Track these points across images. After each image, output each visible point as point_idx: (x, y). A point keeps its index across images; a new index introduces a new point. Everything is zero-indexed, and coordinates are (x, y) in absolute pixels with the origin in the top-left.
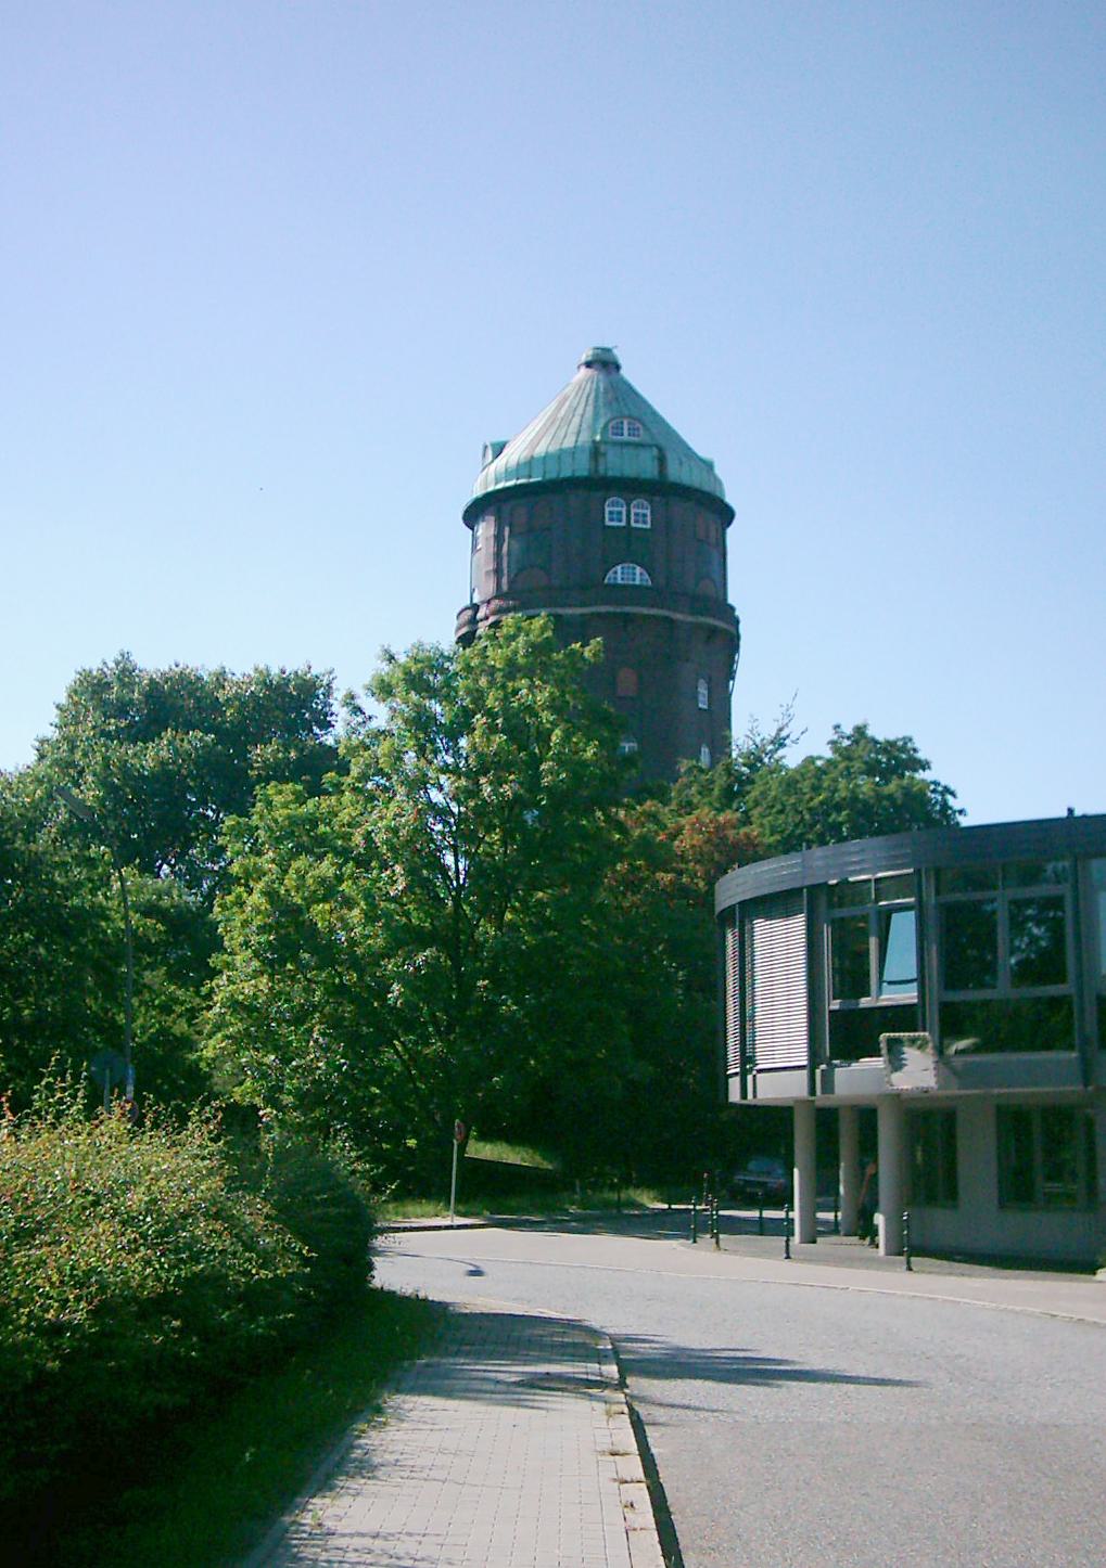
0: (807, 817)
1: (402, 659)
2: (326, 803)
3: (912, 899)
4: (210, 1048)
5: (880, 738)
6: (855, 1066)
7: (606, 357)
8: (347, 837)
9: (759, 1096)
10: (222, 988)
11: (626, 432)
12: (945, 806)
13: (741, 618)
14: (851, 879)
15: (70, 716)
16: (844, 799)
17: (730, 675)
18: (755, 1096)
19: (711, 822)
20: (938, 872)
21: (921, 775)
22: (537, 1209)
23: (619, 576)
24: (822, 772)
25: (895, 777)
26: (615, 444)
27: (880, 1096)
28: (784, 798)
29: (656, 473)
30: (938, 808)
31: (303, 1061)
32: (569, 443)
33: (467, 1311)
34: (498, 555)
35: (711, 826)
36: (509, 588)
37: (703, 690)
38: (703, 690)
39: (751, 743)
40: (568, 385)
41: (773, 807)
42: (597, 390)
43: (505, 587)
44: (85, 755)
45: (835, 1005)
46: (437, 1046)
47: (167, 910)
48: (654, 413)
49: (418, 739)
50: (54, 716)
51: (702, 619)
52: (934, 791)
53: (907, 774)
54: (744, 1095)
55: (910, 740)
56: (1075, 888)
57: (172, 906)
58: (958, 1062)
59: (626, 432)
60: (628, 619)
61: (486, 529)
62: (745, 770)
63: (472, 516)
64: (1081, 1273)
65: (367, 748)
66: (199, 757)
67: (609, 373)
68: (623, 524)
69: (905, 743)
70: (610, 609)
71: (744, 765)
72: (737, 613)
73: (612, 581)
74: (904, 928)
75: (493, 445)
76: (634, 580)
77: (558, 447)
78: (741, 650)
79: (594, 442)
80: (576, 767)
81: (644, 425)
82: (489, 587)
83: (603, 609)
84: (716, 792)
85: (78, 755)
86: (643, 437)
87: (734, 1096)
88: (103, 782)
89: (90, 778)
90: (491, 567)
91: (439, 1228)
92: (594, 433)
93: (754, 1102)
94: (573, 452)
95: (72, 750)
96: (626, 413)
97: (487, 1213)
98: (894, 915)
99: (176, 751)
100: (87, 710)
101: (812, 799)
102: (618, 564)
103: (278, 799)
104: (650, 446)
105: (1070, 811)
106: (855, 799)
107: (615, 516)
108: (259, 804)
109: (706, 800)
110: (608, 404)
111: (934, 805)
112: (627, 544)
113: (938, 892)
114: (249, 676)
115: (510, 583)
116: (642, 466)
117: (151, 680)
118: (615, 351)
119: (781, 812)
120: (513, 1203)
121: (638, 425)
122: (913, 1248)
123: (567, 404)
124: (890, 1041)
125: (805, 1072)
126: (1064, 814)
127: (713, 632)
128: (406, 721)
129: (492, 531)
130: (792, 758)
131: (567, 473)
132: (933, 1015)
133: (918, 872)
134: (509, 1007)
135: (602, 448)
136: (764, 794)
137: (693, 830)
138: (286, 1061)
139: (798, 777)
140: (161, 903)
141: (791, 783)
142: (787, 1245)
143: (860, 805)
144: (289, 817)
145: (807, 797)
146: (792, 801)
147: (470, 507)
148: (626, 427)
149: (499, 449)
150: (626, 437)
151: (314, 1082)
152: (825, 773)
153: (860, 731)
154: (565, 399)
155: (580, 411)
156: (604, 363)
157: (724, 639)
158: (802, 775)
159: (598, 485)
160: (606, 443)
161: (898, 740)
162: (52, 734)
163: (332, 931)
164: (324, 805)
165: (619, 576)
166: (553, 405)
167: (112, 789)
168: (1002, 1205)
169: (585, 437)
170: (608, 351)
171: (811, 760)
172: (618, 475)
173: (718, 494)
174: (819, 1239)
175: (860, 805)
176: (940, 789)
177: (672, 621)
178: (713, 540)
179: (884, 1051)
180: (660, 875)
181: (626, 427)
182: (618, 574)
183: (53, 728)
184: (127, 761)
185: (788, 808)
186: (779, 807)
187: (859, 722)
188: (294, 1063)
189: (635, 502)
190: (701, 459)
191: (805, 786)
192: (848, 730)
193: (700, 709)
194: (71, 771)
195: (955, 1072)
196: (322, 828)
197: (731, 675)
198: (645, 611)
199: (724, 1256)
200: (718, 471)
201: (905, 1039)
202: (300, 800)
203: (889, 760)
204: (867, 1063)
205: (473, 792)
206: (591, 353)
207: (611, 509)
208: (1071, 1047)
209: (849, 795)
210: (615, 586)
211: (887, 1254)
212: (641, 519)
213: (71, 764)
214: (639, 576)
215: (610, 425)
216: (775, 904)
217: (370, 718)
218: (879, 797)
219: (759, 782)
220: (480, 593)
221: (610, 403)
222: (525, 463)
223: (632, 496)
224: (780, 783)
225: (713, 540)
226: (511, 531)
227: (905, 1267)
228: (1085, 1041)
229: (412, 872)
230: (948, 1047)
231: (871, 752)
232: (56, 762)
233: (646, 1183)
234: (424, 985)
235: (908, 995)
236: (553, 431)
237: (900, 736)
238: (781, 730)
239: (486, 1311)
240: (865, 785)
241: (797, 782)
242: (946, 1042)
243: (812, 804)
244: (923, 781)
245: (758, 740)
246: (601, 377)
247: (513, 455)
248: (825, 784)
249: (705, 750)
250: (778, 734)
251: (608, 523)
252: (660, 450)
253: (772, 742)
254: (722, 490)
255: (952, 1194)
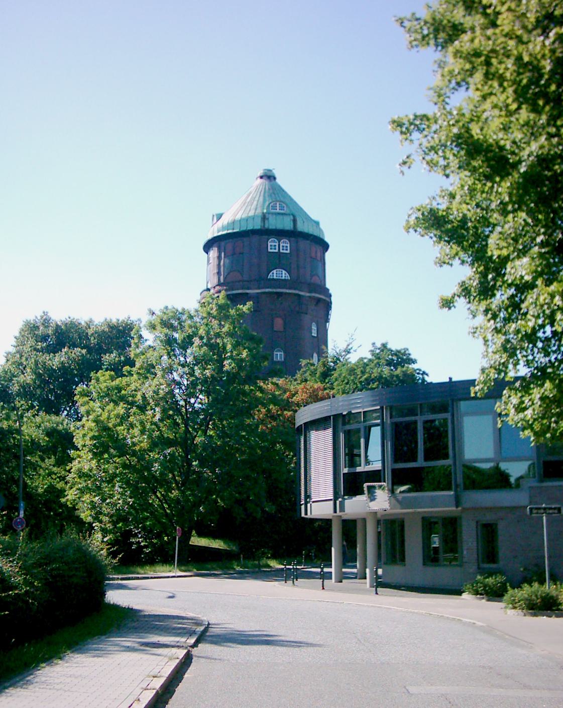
0: (359, 385)
1: (158, 312)
2: (125, 379)
3: (379, 421)
4: (71, 495)
5: (394, 349)
6: (354, 499)
7: (269, 174)
8: (134, 396)
9: (313, 513)
10: (75, 465)
11: (278, 208)
12: (423, 380)
13: (332, 294)
14: (353, 412)
15: (21, 341)
16: (376, 377)
17: (327, 320)
18: (311, 514)
19: (311, 388)
20: (391, 408)
21: (415, 366)
22: (221, 569)
23: (275, 275)
24: (366, 365)
25: (399, 367)
26: (273, 214)
27: (367, 513)
28: (349, 377)
29: (292, 227)
30: (420, 381)
31: (111, 500)
32: (251, 214)
33: (147, 614)
34: (219, 266)
35: (311, 390)
36: (224, 281)
37: (314, 328)
38: (314, 328)
39: (334, 352)
40: (252, 187)
41: (343, 381)
42: (265, 188)
43: (222, 281)
44: (27, 359)
45: (346, 470)
46: (175, 494)
47: (61, 431)
48: (292, 199)
49: (167, 350)
50: (13, 342)
51: (313, 295)
52: (418, 373)
53: (406, 365)
54: (306, 514)
55: (407, 349)
56: (453, 415)
57: (63, 429)
58: (400, 497)
59: (278, 208)
60: (279, 295)
61: (214, 253)
62: (332, 364)
63: (207, 247)
64: (454, 595)
65: (144, 354)
66: (79, 360)
67: (270, 181)
68: (277, 251)
69: (405, 351)
70: (270, 290)
71: (331, 362)
72: (330, 292)
73: (271, 277)
74: (376, 433)
75: (217, 215)
76: (282, 277)
77: (246, 215)
78: (332, 309)
79: (263, 213)
80: (239, 362)
81: (287, 205)
82: (216, 281)
83: (267, 290)
84: (317, 375)
85: (24, 359)
86: (286, 210)
87: (303, 515)
88: (35, 372)
89: (29, 370)
90: (216, 271)
91: (168, 577)
92: (264, 209)
93: (312, 517)
94: (253, 218)
95: (21, 356)
96: (278, 199)
97: (195, 570)
98: (372, 428)
99: (69, 357)
100: (28, 338)
101: (361, 377)
102: (274, 269)
103: (102, 379)
104: (289, 215)
105: (450, 379)
106: (381, 377)
107: (273, 247)
108: (92, 381)
109: (313, 378)
110: (270, 196)
111: (418, 380)
112: (279, 260)
113: (391, 418)
114: (487, 361)
115: (225, 279)
116: (287, 225)
117: (57, 325)
118: (274, 171)
119: (347, 383)
120: (209, 566)
121: (284, 205)
122: (380, 584)
123: (250, 197)
124: (368, 487)
125: (332, 502)
126: (448, 380)
127: (319, 301)
128: (161, 341)
129: (216, 254)
130: (353, 358)
131: (250, 227)
132: (388, 475)
133: (382, 408)
134: (207, 473)
135: (267, 216)
136: (340, 375)
137: (303, 392)
138: (104, 500)
139: (356, 368)
140: (58, 428)
141: (352, 371)
142: (323, 584)
143: (383, 380)
144: (107, 387)
145: (359, 376)
146: (352, 378)
147: (207, 243)
148: (278, 205)
149: (219, 217)
150: (278, 211)
151: (117, 510)
152: (367, 365)
153: (384, 346)
154: (250, 193)
155: (257, 199)
156: (269, 177)
157: (324, 304)
158: (357, 366)
159: (266, 233)
160: (269, 213)
161: (402, 349)
162: (13, 350)
163: (125, 439)
164: (124, 381)
165: (275, 275)
166: (246, 195)
167: (39, 376)
168: (424, 564)
169: (259, 211)
170: (270, 171)
171: (362, 359)
172: (274, 228)
173: (321, 237)
174: (343, 581)
175: (383, 380)
176: (421, 372)
177: (299, 295)
178: (319, 259)
179: (366, 492)
180: (285, 412)
181: (278, 205)
182: (275, 274)
183: (13, 347)
184: (45, 362)
185: (350, 382)
186: (346, 381)
187: (384, 342)
188: (107, 501)
189: (282, 241)
190: (313, 221)
191: (358, 372)
192: (379, 345)
193: (313, 336)
194: (20, 367)
195: (398, 501)
196: (123, 392)
197: (327, 320)
198: (288, 291)
199: (296, 589)
200: (322, 226)
201: (377, 486)
202: (112, 379)
203: (398, 359)
204: (359, 498)
205: (192, 374)
206: (262, 172)
207: (271, 244)
208: (449, 489)
209: (378, 375)
210: (273, 279)
211: (335, 582)
212: (285, 248)
213: (21, 364)
214: (284, 275)
215: (271, 205)
216: (318, 424)
217: (146, 340)
218: (392, 376)
219: (338, 370)
220: (211, 284)
221: (271, 196)
222: (231, 223)
223: (281, 238)
224: (347, 370)
225: (319, 259)
226: (225, 255)
227: (375, 592)
228: (457, 486)
229: (164, 411)
230: (396, 489)
231: (389, 355)
232: (14, 363)
233: (274, 557)
234: (169, 464)
235: (377, 466)
236: (244, 209)
237: (403, 348)
238: (348, 345)
239: (158, 613)
240: (386, 371)
241: (355, 370)
242: (395, 487)
243: (361, 380)
244: (413, 368)
245: (338, 351)
246: (267, 183)
247: (225, 220)
248: (367, 371)
249: (315, 355)
250: (347, 347)
251: (269, 250)
252: (294, 216)
253: (344, 351)
254: (323, 235)
255: (403, 559)
